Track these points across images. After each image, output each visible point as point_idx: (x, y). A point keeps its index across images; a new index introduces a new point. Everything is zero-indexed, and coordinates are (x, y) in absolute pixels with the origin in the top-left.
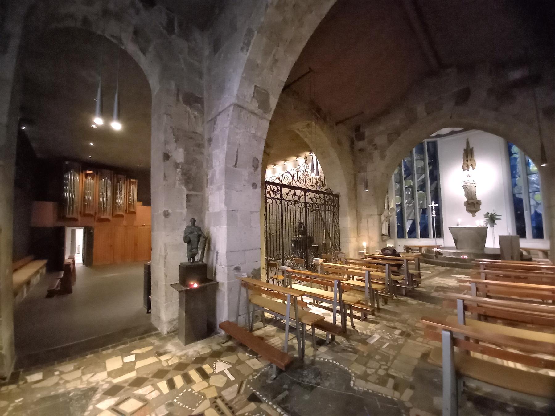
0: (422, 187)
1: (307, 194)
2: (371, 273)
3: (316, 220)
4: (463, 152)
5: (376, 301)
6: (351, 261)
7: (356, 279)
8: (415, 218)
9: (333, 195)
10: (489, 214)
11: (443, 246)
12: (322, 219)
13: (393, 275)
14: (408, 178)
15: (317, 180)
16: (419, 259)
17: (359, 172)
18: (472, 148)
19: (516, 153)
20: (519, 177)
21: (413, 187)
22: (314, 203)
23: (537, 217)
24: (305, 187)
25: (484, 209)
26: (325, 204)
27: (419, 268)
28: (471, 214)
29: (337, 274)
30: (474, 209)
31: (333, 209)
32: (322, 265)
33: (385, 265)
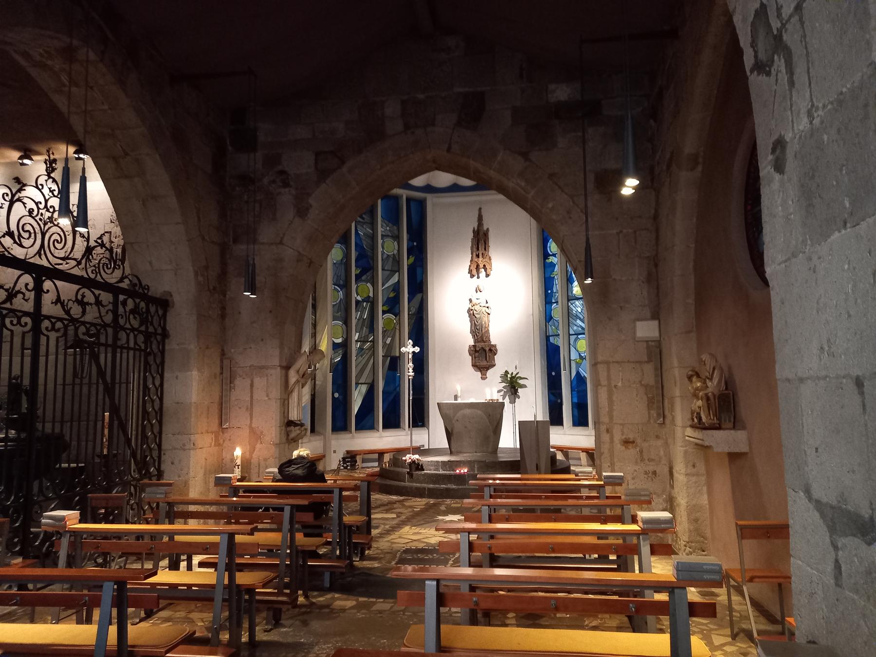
0: (393, 305)
1: (47, 285)
2: (239, 538)
3: (75, 375)
4: (471, 235)
5: (246, 625)
6: (192, 508)
7: (201, 564)
8: (373, 381)
9: (151, 300)
10: (509, 376)
11: (427, 448)
12: (101, 373)
13: (306, 535)
14: (364, 278)
15: (92, 243)
16: (369, 483)
17: (236, 241)
18: (488, 229)
19: (554, 255)
20: (557, 302)
21: (372, 302)
22: (73, 320)
23: (579, 382)
24: (36, 261)
25: (503, 363)
26: (117, 327)
27: (367, 508)
28: (479, 374)
29: (140, 556)
30: (484, 363)
31: (145, 342)
32: (75, 533)
33: (281, 509)
